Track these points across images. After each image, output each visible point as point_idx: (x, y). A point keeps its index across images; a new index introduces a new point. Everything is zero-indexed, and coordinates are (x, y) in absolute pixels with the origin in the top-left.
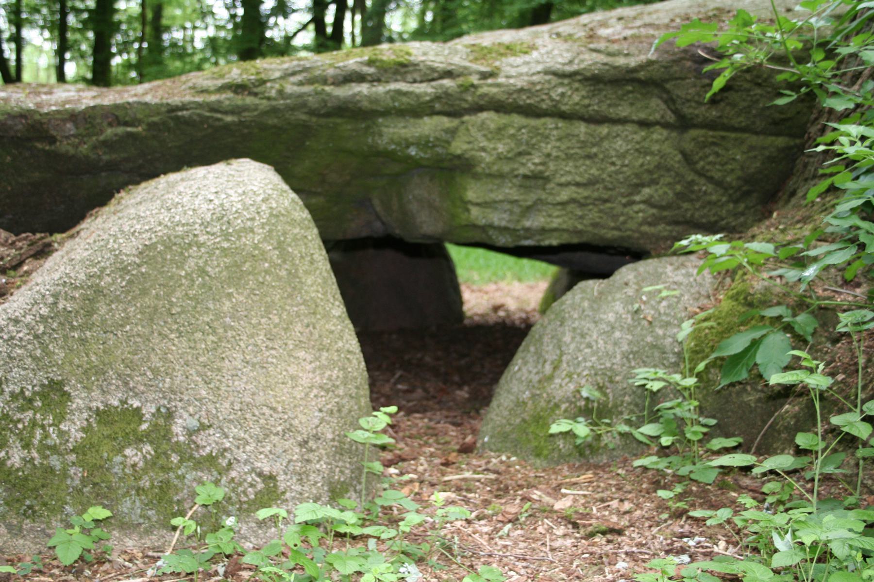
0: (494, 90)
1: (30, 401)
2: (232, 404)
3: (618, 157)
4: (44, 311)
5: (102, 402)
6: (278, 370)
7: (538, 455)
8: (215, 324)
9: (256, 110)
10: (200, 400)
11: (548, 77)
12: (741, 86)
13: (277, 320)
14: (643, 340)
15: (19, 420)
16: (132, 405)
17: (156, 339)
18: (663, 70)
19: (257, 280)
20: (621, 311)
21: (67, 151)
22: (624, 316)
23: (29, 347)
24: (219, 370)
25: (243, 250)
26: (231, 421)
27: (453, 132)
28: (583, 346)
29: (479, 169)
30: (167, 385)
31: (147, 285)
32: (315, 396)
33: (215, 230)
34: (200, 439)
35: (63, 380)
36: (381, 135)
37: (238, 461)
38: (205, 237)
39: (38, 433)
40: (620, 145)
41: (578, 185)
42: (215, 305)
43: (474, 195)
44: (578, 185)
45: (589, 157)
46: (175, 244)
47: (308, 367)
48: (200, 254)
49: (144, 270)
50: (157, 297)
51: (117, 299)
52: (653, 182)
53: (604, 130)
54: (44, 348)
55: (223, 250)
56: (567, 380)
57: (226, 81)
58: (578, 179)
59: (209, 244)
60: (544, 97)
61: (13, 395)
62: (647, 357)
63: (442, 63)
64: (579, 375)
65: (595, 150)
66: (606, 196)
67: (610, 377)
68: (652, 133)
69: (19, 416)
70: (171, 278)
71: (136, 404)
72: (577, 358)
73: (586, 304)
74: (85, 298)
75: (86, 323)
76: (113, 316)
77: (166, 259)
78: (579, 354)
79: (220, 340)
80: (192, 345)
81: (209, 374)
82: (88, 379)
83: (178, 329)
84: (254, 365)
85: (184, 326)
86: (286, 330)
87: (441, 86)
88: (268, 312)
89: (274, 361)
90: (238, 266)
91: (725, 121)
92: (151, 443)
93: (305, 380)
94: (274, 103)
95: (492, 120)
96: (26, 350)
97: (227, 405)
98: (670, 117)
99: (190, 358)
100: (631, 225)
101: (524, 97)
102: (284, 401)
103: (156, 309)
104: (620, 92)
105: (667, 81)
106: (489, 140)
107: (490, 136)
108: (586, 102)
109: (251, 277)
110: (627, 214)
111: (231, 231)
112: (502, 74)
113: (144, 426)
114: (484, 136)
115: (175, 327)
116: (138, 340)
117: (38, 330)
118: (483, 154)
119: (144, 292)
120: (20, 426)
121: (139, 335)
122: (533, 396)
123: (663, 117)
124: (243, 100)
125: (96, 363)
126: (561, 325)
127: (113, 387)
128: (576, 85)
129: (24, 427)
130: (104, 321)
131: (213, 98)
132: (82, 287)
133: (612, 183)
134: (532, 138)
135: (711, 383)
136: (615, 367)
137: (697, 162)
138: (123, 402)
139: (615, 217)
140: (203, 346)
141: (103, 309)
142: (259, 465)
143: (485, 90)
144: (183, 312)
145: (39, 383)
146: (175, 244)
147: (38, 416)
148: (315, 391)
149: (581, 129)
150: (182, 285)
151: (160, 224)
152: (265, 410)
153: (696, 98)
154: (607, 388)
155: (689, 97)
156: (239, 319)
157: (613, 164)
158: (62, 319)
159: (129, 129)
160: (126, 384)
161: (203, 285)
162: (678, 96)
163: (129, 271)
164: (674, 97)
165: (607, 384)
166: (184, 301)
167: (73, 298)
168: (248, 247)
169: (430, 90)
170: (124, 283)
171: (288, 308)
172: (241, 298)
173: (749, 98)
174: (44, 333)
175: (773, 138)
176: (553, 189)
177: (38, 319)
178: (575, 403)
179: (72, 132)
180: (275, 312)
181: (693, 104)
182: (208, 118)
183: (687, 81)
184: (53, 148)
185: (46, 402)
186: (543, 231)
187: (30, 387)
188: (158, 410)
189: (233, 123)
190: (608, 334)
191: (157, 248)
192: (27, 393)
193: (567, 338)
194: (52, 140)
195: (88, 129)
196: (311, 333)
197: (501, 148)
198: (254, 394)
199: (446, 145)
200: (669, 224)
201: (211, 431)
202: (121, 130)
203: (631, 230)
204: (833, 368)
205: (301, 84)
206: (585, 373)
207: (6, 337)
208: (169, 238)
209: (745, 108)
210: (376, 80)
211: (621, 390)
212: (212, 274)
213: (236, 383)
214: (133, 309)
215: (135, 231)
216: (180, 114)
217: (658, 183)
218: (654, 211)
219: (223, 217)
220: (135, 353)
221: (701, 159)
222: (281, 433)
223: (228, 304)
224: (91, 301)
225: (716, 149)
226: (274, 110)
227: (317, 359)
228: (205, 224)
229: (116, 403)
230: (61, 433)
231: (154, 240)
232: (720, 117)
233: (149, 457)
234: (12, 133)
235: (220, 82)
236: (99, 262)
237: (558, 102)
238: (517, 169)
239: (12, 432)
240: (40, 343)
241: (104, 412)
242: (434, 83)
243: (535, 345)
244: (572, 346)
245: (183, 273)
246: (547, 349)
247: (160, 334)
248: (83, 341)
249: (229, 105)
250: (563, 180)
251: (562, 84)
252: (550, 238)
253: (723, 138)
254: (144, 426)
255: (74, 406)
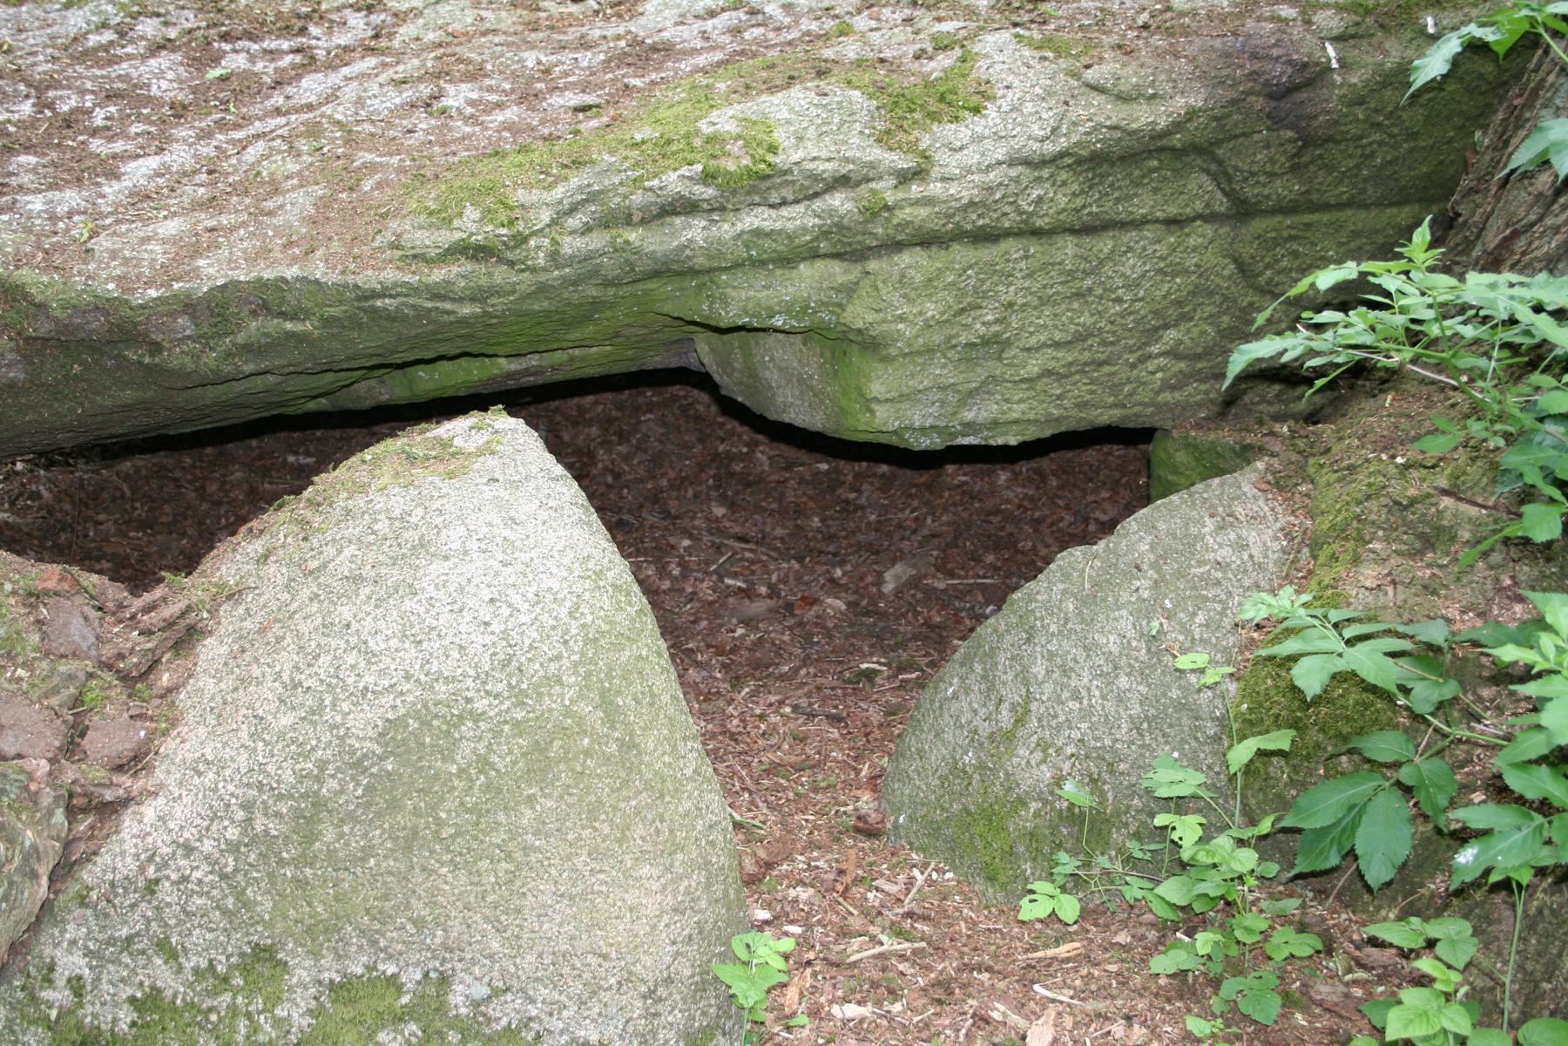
0: (923, 212)
1: (225, 980)
2: (540, 956)
3: (1127, 287)
4: (233, 833)
5: (338, 972)
6: (610, 901)
7: (991, 879)
8: (511, 846)
9: (513, 292)
10: (490, 956)
11: (1013, 172)
12: (1347, 132)
13: (607, 830)
14: (1164, 695)
15: (211, 1010)
16: (384, 972)
17: (418, 877)
18: (1214, 124)
19: (573, 770)
20: (1131, 634)
21: (184, 365)
22: (1134, 644)
23: (214, 892)
24: (518, 911)
25: (548, 720)
26: (537, 980)
27: (850, 290)
28: (1065, 695)
29: (893, 351)
30: (438, 940)
31: (398, 793)
32: (667, 926)
33: (500, 687)
34: (493, 1010)
35: (273, 944)
36: (724, 300)
37: (551, 1032)
38: (485, 702)
39: (242, 1025)
40: (1132, 266)
41: (1057, 345)
42: (509, 816)
43: (883, 389)
44: (1057, 345)
45: (1078, 295)
46: (436, 716)
47: (656, 886)
48: (478, 733)
49: (390, 768)
50: (416, 812)
51: (352, 817)
52: (1185, 317)
53: (1105, 244)
54: (240, 895)
55: (516, 724)
56: (1039, 755)
57: (457, 236)
58: (1058, 336)
59: (492, 714)
60: (1008, 209)
61: (196, 971)
62: (1170, 726)
63: (829, 160)
64: (1059, 751)
65: (1088, 282)
66: (1102, 357)
67: (1110, 765)
68: (1188, 235)
69: (209, 1003)
70: (436, 777)
71: (391, 969)
72: (1055, 716)
73: (1070, 606)
74: (297, 814)
75: (303, 855)
76: (347, 844)
77: (423, 745)
78: (1058, 709)
79: (518, 868)
80: (476, 879)
81: (503, 918)
82: (314, 940)
83: (452, 861)
84: (572, 898)
85: (460, 854)
86: (619, 841)
87: (832, 212)
88: (593, 817)
89: (604, 888)
90: (542, 751)
91: (1314, 197)
92: (417, 1020)
93: (650, 907)
94: (542, 277)
95: (917, 267)
96: (211, 898)
97: (531, 958)
98: (1221, 204)
99: (472, 899)
100: (1144, 395)
101: (974, 217)
102: (619, 943)
103: (415, 831)
104: (1137, 173)
105: (1219, 143)
106: (911, 301)
107: (913, 295)
108: (1079, 202)
109: (562, 766)
110: (1137, 379)
111: (524, 686)
112: (936, 172)
113: (405, 1000)
114: (905, 296)
115: (448, 857)
116: (389, 879)
117: (226, 866)
118: (901, 326)
119: (394, 806)
120: (213, 1017)
121: (390, 873)
122: (981, 767)
123: (1207, 205)
124: (490, 274)
125: (325, 916)
126: (1028, 640)
127: (354, 949)
128: (1064, 175)
129: (220, 1020)
130: (331, 853)
131: (438, 275)
132: (291, 797)
133: (1114, 333)
134: (983, 281)
135: (1272, 782)
136: (1118, 746)
137: (1260, 274)
138: (370, 968)
139: (1115, 389)
140: (493, 879)
141: (329, 834)
142: (583, 1033)
143: (905, 214)
144: (458, 834)
145: (236, 951)
146: (436, 716)
147: (240, 1000)
148: (666, 918)
149: (1068, 248)
150: (453, 789)
151: (407, 677)
152: (591, 959)
153: (1268, 168)
154: (1105, 782)
155: (1255, 168)
156: (547, 836)
157: (1119, 300)
158: (263, 848)
159: (289, 326)
160: (374, 943)
161: (488, 787)
162: (1236, 169)
163: (366, 770)
164: (1231, 171)
165: (1106, 776)
166: (458, 815)
167: (278, 815)
168: (556, 714)
169: (811, 222)
170: (360, 792)
171: (622, 805)
172: (550, 804)
173: (1359, 151)
174: (236, 870)
175: (1394, 210)
176: (1014, 357)
177: (223, 847)
178: (1052, 803)
179: (188, 332)
180: (603, 817)
181: (1262, 179)
182: (430, 310)
183: (1256, 137)
184: (157, 360)
185: (250, 979)
186: (995, 424)
187: (223, 958)
188: (426, 975)
189: (474, 316)
190: (1108, 678)
191: (407, 726)
192: (219, 968)
193: (1039, 669)
194: (156, 348)
195: (215, 325)
196: (658, 832)
197: (931, 310)
198: (573, 938)
199: (838, 310)
200: (1202, 381)
201: (509, 997)
202: (274, 325)
203: (1140, 404)
204: (1467, 774)
205: (587, 229)
206: (1069, 750)
207: (174, 877)
208: (425, 706)
209: (1350, 169)
210: (718, 209)
211: (1128, 788)
212: (500, 766)
213: (546, 926)
214: (378, 832)
215: (366, 688)
216: (379, 303)
217: (1191, 319)
218: (1182, 365)
219: (510, 661)
220: (386, 897)
221: (1268, 266)
222: (615, 987)
223: (528, 813)
224: (310, 821)
225: (1295, 246)
226: (543, 289)
227: (668, 869)
228: (483, 678)
229: (359, 970)
230: (278, 1022)
231: (402, 711)
232: (1307, 192)
233: (413, 1040)
234: (82, 335)
235: (446, 238)
236: (313, 749)
237: (1030, 215)
238: (957, 336)
239: (201, 1028)
240: (230, 886)
241: (342, 986)
242: (817, 204)
243: (981, 662)
244: (1048, 688)
245: (454, 769)
246: (1004, 677)
247: (424, 869)
248: (301, 883)
249: (465, 288)
250: (1033, 341)
251: (1039, 179)
252: (1006, 433)
253: (1308, 226)
254: (405, 1000)
255: (295, 980)
